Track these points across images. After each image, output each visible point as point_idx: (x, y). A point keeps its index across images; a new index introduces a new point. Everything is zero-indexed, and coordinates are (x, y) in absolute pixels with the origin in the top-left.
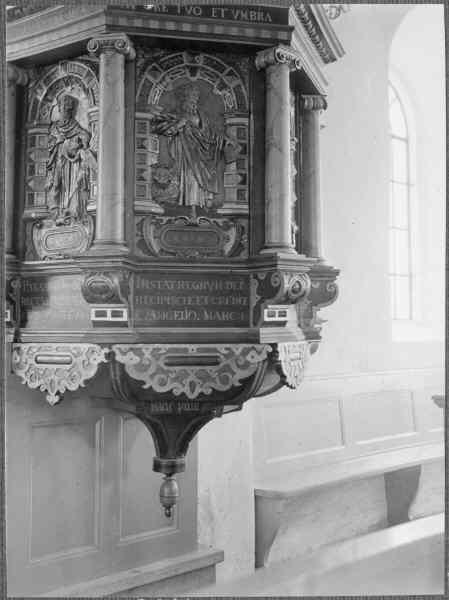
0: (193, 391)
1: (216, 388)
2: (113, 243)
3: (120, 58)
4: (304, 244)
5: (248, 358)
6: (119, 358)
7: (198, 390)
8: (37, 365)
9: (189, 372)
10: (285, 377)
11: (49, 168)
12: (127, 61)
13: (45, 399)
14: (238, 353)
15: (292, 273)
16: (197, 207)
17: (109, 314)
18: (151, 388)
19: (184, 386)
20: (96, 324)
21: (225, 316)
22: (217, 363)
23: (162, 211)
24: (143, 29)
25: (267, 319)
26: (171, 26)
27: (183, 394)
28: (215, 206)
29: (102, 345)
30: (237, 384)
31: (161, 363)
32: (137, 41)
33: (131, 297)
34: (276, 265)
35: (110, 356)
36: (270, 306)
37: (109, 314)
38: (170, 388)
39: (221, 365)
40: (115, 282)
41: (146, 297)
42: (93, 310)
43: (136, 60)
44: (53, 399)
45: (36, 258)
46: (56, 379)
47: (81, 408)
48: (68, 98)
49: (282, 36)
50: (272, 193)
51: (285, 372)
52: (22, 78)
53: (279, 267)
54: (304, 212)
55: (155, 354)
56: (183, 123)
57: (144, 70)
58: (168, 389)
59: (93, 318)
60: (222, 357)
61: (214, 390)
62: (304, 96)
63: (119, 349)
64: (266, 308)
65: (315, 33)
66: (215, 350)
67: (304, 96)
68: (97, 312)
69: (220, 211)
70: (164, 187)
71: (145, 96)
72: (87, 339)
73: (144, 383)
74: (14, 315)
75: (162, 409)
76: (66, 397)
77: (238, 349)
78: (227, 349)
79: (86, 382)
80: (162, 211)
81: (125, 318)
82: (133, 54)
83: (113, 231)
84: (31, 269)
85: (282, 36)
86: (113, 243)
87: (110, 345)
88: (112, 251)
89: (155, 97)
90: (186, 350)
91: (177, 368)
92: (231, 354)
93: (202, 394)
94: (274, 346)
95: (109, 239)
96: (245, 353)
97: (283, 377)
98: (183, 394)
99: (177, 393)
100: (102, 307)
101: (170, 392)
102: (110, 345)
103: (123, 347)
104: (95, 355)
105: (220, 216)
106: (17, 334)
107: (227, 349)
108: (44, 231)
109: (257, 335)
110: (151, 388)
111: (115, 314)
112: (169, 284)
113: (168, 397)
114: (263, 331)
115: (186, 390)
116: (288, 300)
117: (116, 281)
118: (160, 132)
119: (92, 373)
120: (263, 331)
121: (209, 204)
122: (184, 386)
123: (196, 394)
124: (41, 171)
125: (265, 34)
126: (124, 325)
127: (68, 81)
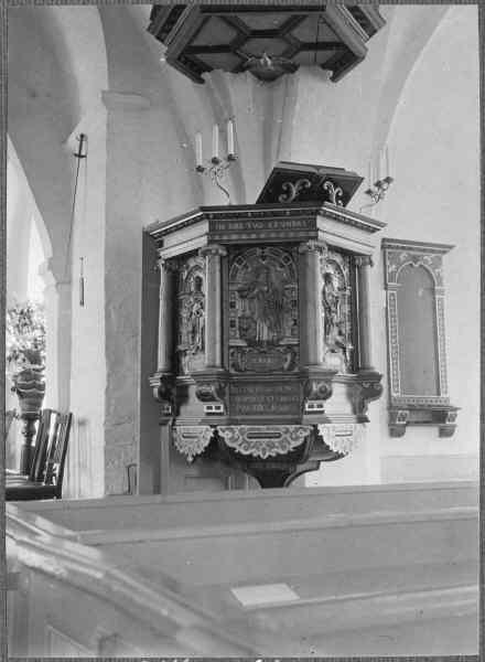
0: (264, 454)
2: (214, 366)
3: (217, 258)
6: (221, 434)
7: (267, 454)
11: (189, 320)
12: (222, 258)
14: (291, 430)
15: (318, 381)
16: (268, 342)
20: (209, 414)
21: (286, 408)
23: (245, 344)
24: (229, 240)
26: (244, 237)
28: (278, 340)
29: (212, 426)
31: (245, 437)
32: (228, 247)
33: (227, 398)
35: (216, 432)
40: (212, 389)
44: (190, 459)
45: (183, 374)
46: (191, 446)
47: (199, 460)
48: (198, 277)
49: (312, 234)
50: (167, 333)
52: (175, 267)
55: (241, 431)
56: (256, 290)
57: (234, 260)
59: (206, 411)
66: (278, 429)
69: (281, 343)
70: (247, 330)
71: (234, 276)
72: (203, 422)
74: (173, 410)
76: (196, 457)
77: (292, 428)
79: (206, 448)
80: (245, 344)
81: (222, 410)
82: (225, 253)
83: (214, 360)
84: (181, 381)
85: (312, 234)
86: (214, 366)
87: (215, 426)
88: (215, 370)
89: (240, 277)
90: (258, 429)
91: (254, 440)
92: (287, 431)
93: (270, 456)
94: (315, 426)
95: (212, 364)
96: (297, 430)
99: (255, 455)
100: (210, 404)
102: (215, 426)
103: (223, 427)
105: (283, 346)
106: (174, 420)
108: (187, 358)
109: (301, 419)
114: (305, 417)
115: (261, 453)
117: (213, 388)
118: (242, 297)
119: (206, 443)
121: (275, 338)
124: (185, 321)
125: (302, 234)
126: (220, 414)
127: (197, 267)
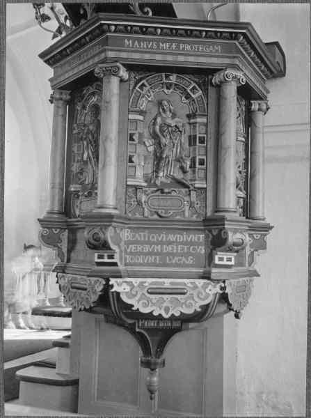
1: (183, 311)
4: (247, 208)
5: (207, 291)
8: (149, 295)
9: (165, 299)
10: (231, 305)
12: (122, 81)
13: (155, 316)
17: (225, 260)
18: (138, 309)
19: (161, 309)
22: (184, 294)
25: (217, 262)
27: (160, 315)
30: (199, 310)
34: (224, 225)
36: (219, 253)
37: (225, 260)
38: (152, 309)
39: (188, 294)
41: (175, 251)
42: (96, 254)
43: (129, 80)
51: (231, 302)
53: (226, 226)
54: (248, 182)
58: (149, 311)
60: (188, 289)
61: (181, 312)
62: (252, 102)
63: (117, 282)
64: (217, 254)
65: (94, 34)
67: (252, 102)
68: (99, 255)
73: (133, 306)
75: (152, 324)
78: (191, 283)
81: (233, 263)
97: (230, 305)
98: (160, 315)
99: (155, 314)
100: (101, 252)
101: (151, 313)
104: (210, 287)
107: (191, 283)
109: (210, 273)
110: (138, 309)
111: (229, 260)
112: (140, 236)
113: (150, 316)
114: (214, 270)
116: (230, 250)
120: (214, 270)
122: (161, 309)
123: (169, 315)
